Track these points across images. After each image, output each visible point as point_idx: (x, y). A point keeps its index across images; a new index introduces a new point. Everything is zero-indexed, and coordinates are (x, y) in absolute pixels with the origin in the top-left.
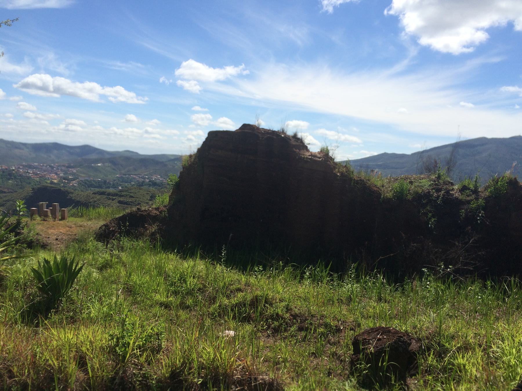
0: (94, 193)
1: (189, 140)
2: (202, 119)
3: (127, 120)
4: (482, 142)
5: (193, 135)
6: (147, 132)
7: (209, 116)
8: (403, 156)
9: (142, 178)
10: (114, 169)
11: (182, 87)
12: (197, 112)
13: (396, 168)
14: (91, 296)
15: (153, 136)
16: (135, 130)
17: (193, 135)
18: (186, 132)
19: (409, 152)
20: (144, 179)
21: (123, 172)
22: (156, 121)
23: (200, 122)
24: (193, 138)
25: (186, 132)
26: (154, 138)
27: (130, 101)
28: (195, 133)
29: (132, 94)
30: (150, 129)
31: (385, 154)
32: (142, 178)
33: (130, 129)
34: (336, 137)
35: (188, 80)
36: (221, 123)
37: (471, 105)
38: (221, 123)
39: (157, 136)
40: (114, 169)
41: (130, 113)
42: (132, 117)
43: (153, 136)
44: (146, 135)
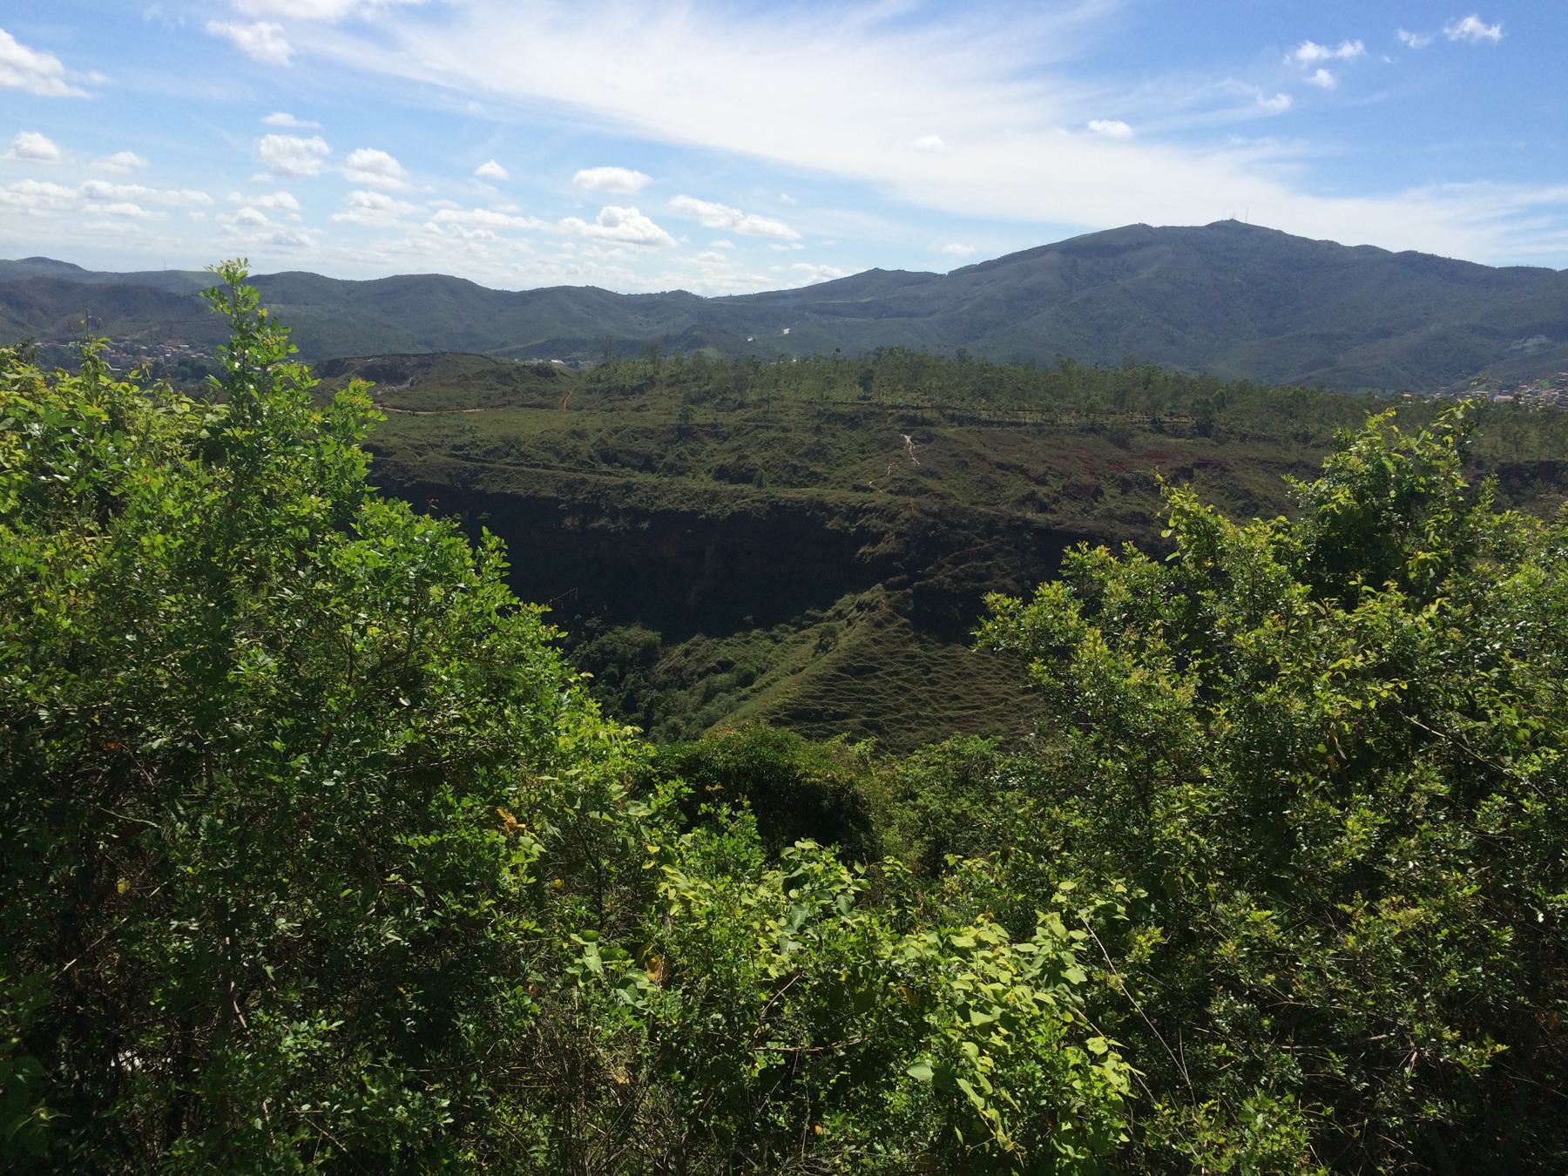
0: (872, 490)
1: (250, 223)
2: (295, 153)
3: (20, 154)
4: (1136, 239)
5: (261, 209)
6: (92, 195)
7: (318, 144)
8: (926, 279)
9: (125, 350)
10: (16, 322)
11: (225, 44)
12: (279, 130)
13: (911, 315)
14: (1485, 1047)
15: (115, 208)
16: (51, 188)
17: (261, 209)
18: (235, 197)
19: (943, 269)
20: (134, 353)
21: (52, 330)
22: (126, 157)
23: (290, 164)
24: (259, 216)
25: (235, 197)
26: (123, 216)
27: (39, 89)
28: (268, 201)
29: (48, 63)
30: (103, 186)
31: (876, 274)
32: (125, 350)
33: (31, 185)
34: (724, 221)
35: (249, 21)
36: (362, 169)
37: (1122, 128)
38: (362, 169)
39: (134, 209)
40: (16, 322)
41: (31, 129)
42: (38, 143)
43: (115, 208)
44: (92, 207)
